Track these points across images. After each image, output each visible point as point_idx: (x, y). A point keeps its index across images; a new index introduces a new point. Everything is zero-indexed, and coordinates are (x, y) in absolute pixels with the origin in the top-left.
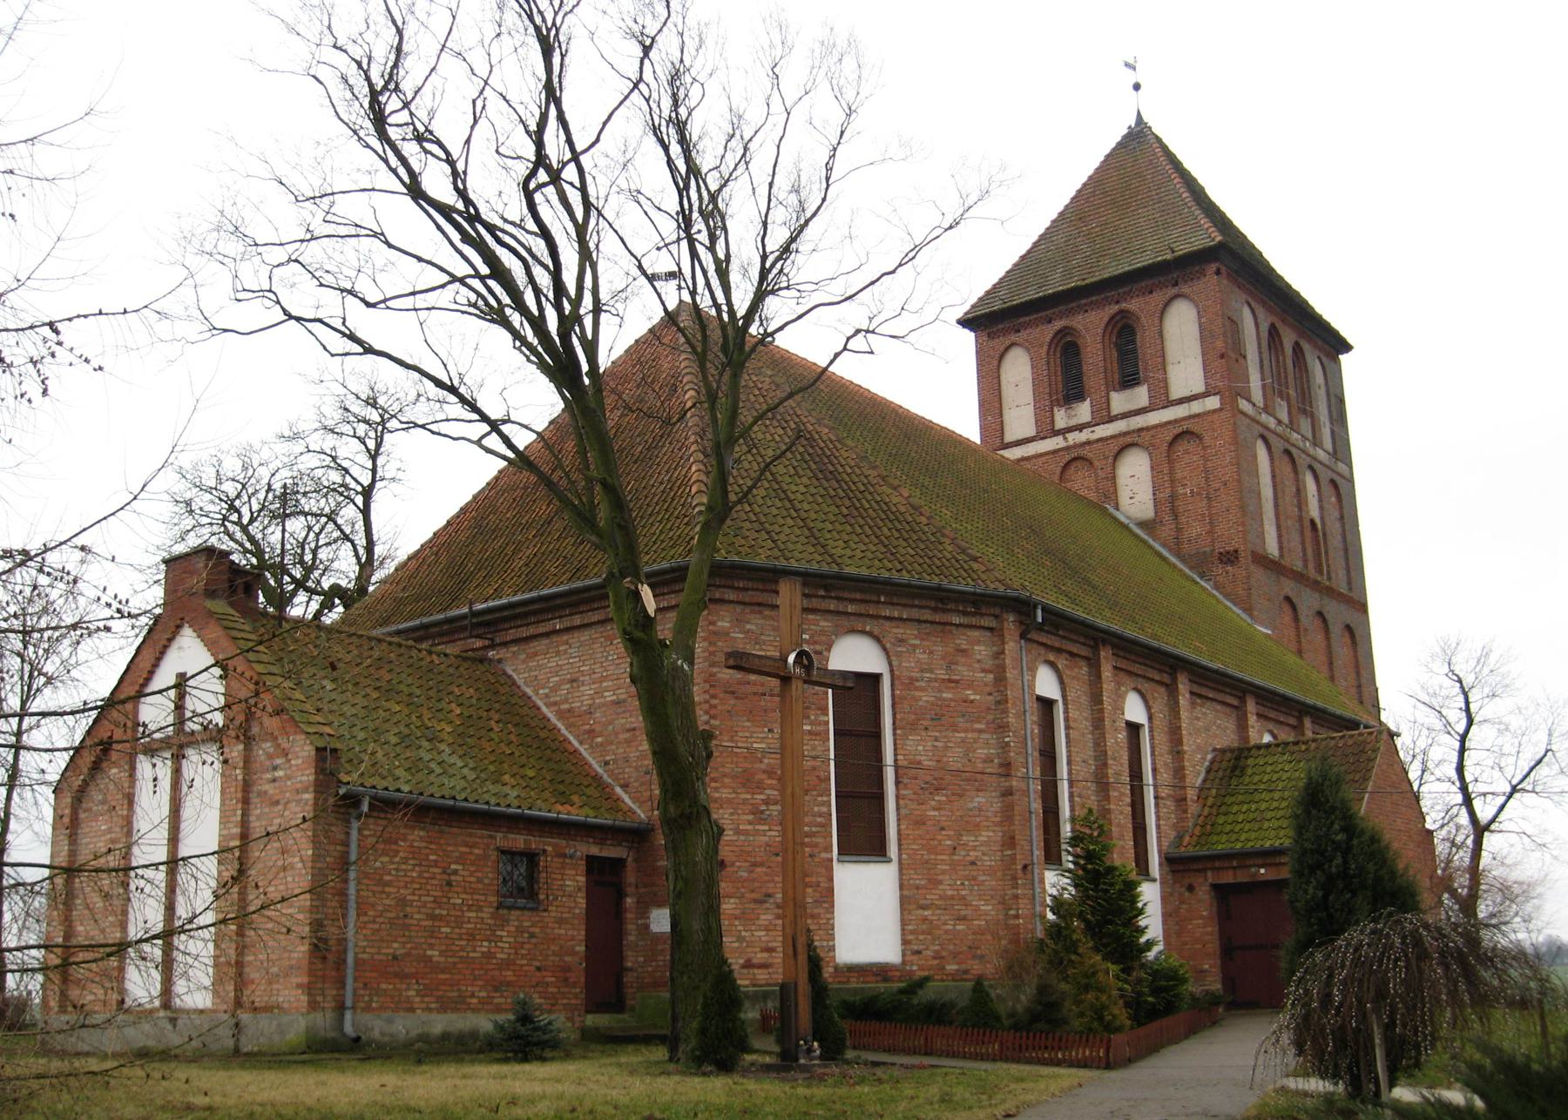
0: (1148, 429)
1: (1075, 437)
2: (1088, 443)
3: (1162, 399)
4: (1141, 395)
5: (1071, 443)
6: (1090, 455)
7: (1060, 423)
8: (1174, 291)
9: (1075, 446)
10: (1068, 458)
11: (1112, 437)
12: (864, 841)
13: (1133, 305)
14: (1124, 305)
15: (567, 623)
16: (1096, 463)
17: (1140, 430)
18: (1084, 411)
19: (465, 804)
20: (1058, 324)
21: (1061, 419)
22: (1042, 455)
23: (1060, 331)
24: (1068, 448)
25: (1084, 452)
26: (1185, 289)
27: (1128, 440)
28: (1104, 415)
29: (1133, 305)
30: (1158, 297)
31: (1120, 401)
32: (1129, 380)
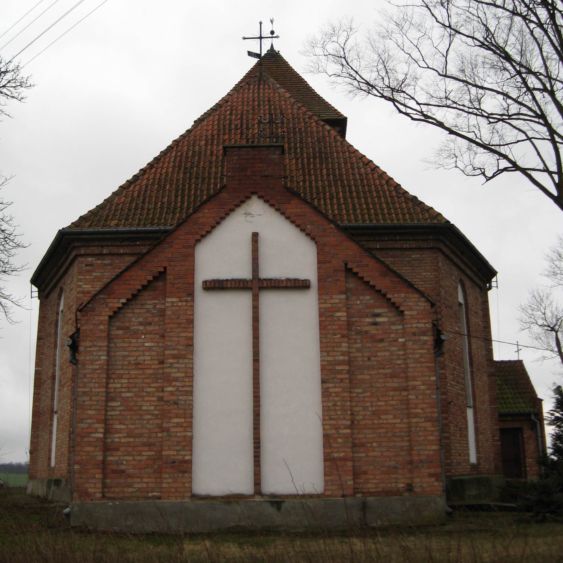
15: (115, 250)
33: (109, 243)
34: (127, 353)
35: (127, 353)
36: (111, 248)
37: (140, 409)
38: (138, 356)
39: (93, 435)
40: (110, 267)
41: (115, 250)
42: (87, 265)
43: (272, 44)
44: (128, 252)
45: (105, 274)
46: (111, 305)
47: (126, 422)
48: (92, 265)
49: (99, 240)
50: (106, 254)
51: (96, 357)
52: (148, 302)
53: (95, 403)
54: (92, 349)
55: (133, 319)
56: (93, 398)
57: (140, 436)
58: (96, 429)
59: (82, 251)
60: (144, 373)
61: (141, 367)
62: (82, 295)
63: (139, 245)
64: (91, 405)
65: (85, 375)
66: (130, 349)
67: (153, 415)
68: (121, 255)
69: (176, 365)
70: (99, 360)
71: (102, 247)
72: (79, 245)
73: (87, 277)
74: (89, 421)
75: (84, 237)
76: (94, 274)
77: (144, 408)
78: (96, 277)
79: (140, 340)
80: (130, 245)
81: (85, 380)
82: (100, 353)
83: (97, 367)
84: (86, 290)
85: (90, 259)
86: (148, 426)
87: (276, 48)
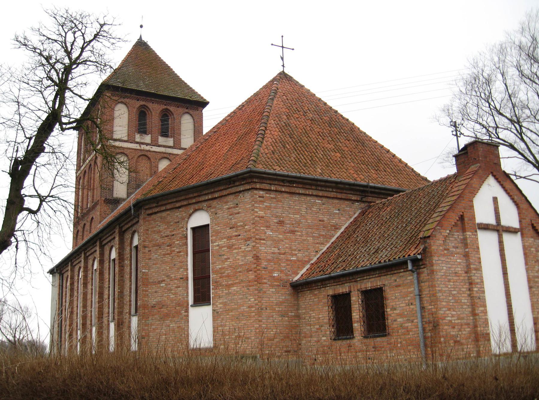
0: (173, 154)
1: (143, 147)
2: (149, 151)
3: (177, 145)
4: (170, 142)
5: (142, 148)
6: (149, 156)
7: (138, 140)
8: (187, 110)
9: (143, 150)
10: (140, 154)
11: (159, 152)
12: (202, 298)
13: (150, 105)
14: (168, 107)
15: (279, 188)
16: (152, 159)
17: (170, 154)
18: (147, 139)
19: (390, 263)
20: (142, 103)
21: (138, 138)
22: (130, 149)
23: (142, 106)
24: (141, 150)
25: (148, 154)
26: (191, 112)
27: (165, 155)
28: (154, 143)
29: (150, 105)
30: (181, 110)
31: (161, 140)
32: (165, 133)
33: (276, 183)
34: (450, 266)
35: (450, 266)
36: (276, 186)
37: (461, 302)
38: (456, 268)
39: (447, 318)
40: (275, 200)
41: (279, 188)
42: (260, 197)
43: (141, 36)
44: (287, 190)
45: (272, 205)
46: (443, 234)
47: (457, 310)
48: (263, 197)
49: (270, 179)
50: (273, 191)
51: (442, 268)
52: (455, 234)
53: (445, 297)
54: (438, 262)
55: (450, 244)
56: (444, 294)
57: (463, 319)
58: (448, 314)
59: (258, 186)
60: (459, 279)
61: (458, 275)
62: (258, 219)
63: (295, 187)
64: (443, 299)
65: (438, 278)
66: (451, 263)
67: (467, 305)
68: (282, 192)
69: (476, 275)
70: (443, 269)
71: (270, 184)
72: (257, 181)
73: (261, 206)
74: (444, 309)
75: (264, 176)
76: (265, 204)
77: (463, 301)
78: (266, 206)
79: (455, 258)
80: (290, 186)
81: (439, 282)
82: (443, 265)
83: (443, 274)
84: (261, 215)
85: (261, 192)
86: (466, 313)
87: (144, 39)
